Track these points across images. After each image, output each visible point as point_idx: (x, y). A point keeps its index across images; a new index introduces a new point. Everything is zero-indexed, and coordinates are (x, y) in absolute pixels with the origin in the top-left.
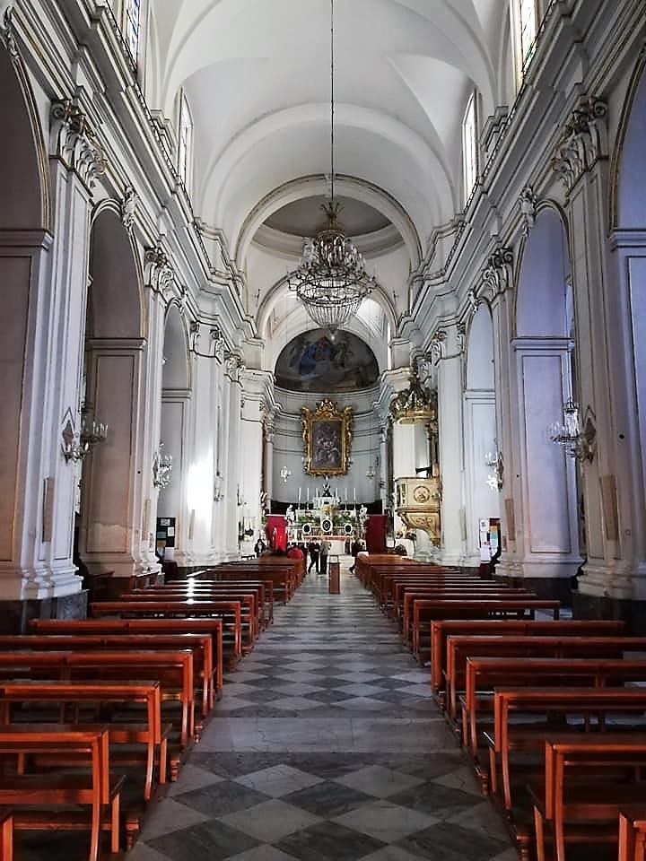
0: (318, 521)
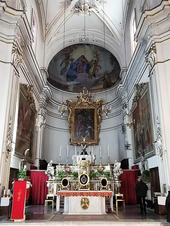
0: (76, 175)
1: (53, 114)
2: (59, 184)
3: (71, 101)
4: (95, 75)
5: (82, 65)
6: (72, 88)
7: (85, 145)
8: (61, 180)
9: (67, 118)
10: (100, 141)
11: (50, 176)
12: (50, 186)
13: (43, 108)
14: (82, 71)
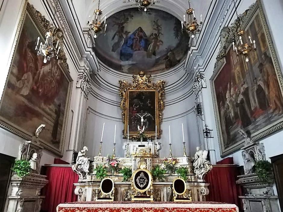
0: (128, 173)
1: (101, 97)
2: (97, 188)
3: (125, 82)
4: (155, 54)
5: (139, 41)
6: (127, 69)
7: (144, 127)
8: (100, 182)
9: (120, 103)
10: (162, 134)
11: (81, 173)
12: (79, 193)
13: (83, 78)
14: (139, 49)
